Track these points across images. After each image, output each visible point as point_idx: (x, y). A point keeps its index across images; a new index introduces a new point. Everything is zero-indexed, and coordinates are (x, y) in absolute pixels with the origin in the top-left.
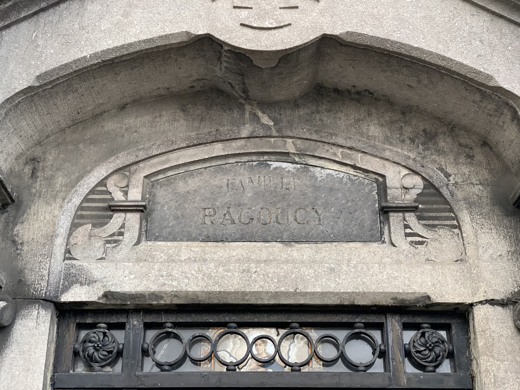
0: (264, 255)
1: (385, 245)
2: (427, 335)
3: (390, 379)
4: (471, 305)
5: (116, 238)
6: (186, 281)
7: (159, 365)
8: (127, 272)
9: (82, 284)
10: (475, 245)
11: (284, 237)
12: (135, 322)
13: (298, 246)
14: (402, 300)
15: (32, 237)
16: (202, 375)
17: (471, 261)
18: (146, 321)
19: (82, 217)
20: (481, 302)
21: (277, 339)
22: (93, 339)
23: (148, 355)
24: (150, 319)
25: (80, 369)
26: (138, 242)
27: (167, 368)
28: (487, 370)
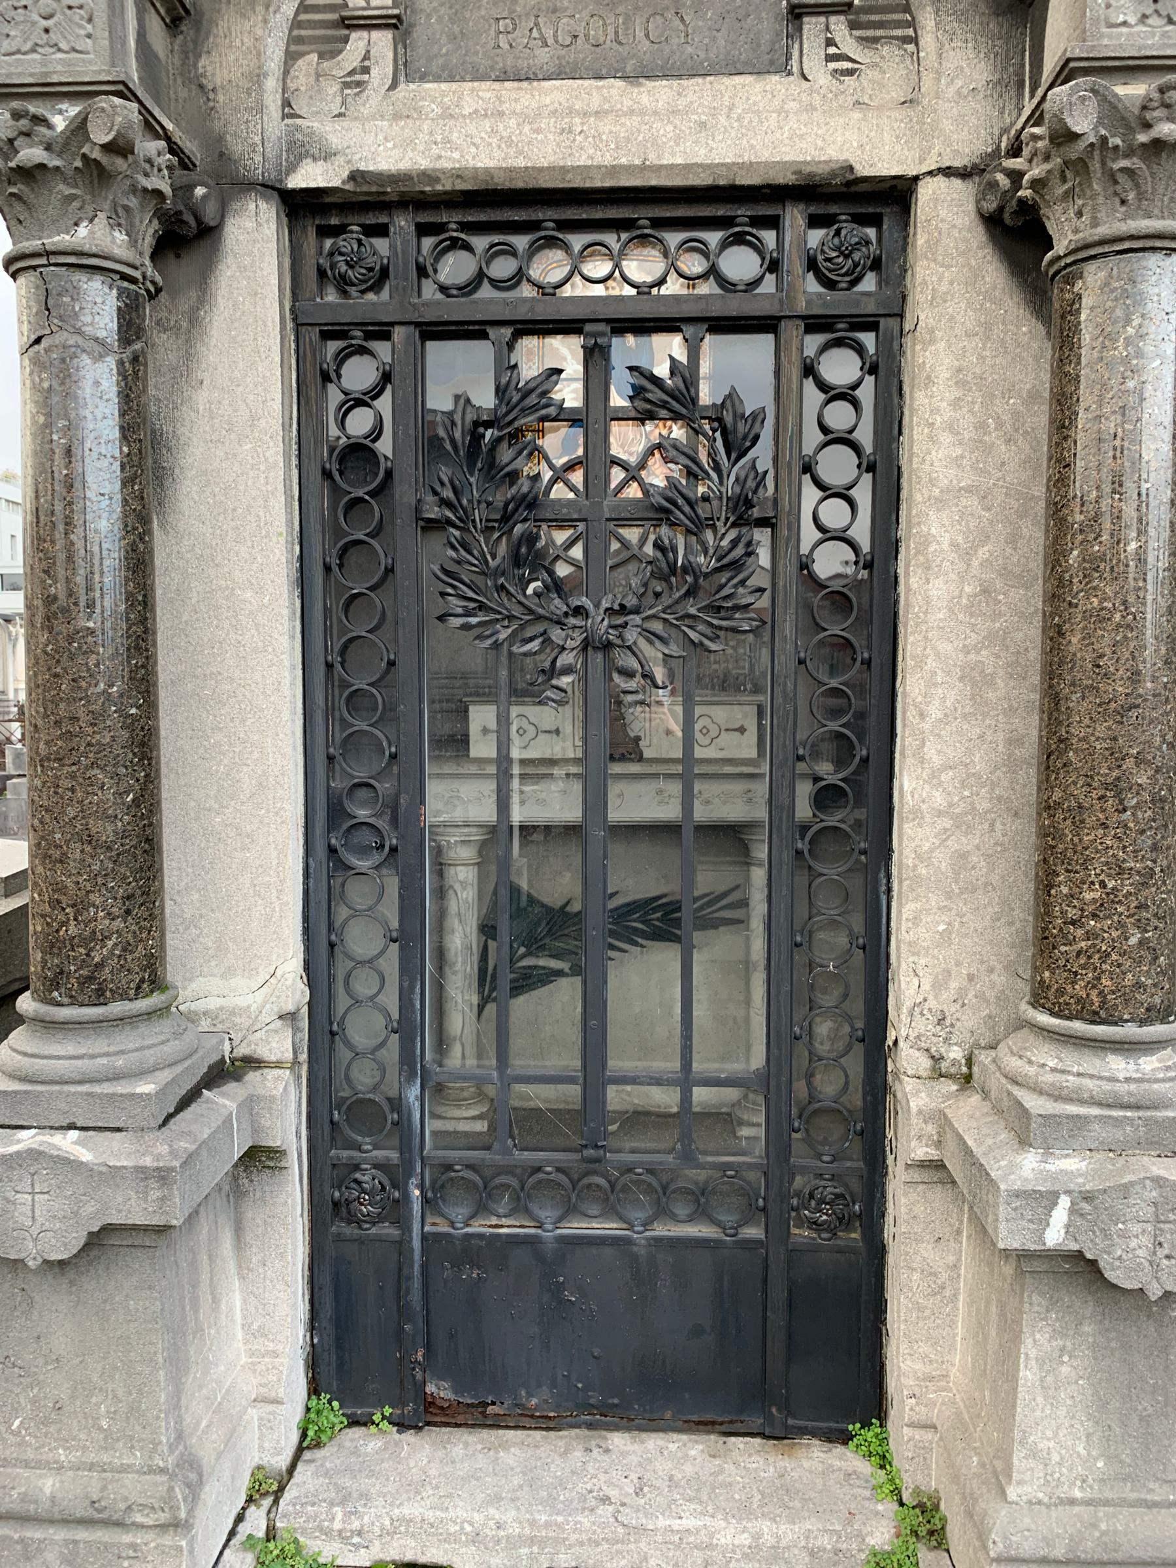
0: (595, 103)
1: (791, 78)
2: (843, 232)
3: (781, 301)
4: (916, 179)
5: (358, 77)
6: (473, 150)
7: (443, 289)
8: (381, 137)
9: (315, 159)
10: (937, 72)
11: (628, 69)
12: (403, 223)
13: (649, 84)
14: (809, 174)
15: (227, 78)
16: (506, 303)
17: (925, 102)
18: (418, 220)
19: (300, 40)
20: (930, 173)
21: (616, 247)
22: (343, 250)
23: (427, 276)
24: (426, 217)
25: (331, 296)
26: (394, 86)
27: (454, 292)
28: (924, 282)
